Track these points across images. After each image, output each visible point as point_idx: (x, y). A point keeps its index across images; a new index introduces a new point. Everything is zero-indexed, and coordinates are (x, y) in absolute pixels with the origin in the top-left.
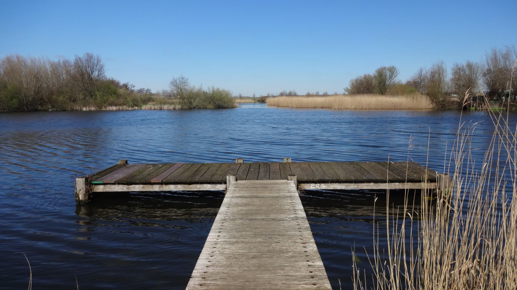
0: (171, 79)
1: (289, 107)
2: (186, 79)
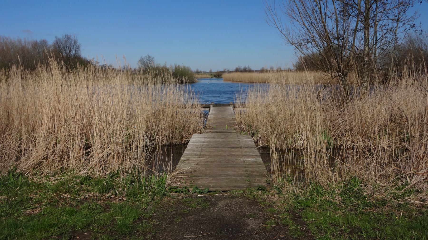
0: (139, 58)
1: (242, 82)
2: (152, 57)
